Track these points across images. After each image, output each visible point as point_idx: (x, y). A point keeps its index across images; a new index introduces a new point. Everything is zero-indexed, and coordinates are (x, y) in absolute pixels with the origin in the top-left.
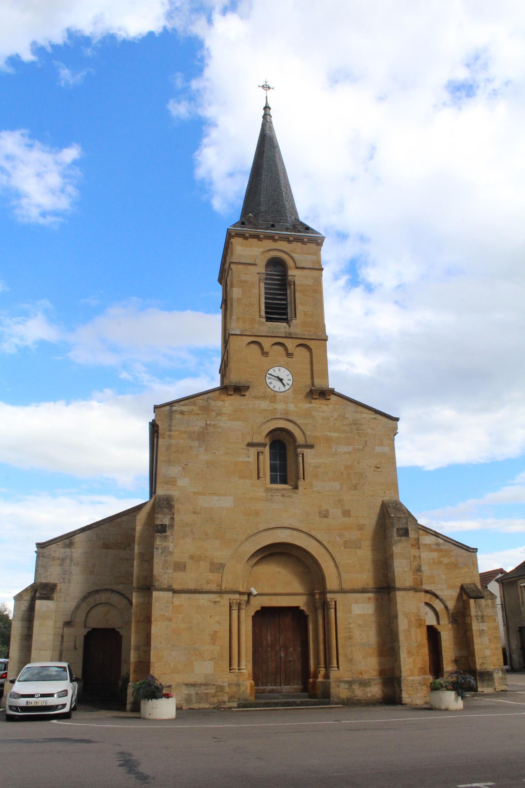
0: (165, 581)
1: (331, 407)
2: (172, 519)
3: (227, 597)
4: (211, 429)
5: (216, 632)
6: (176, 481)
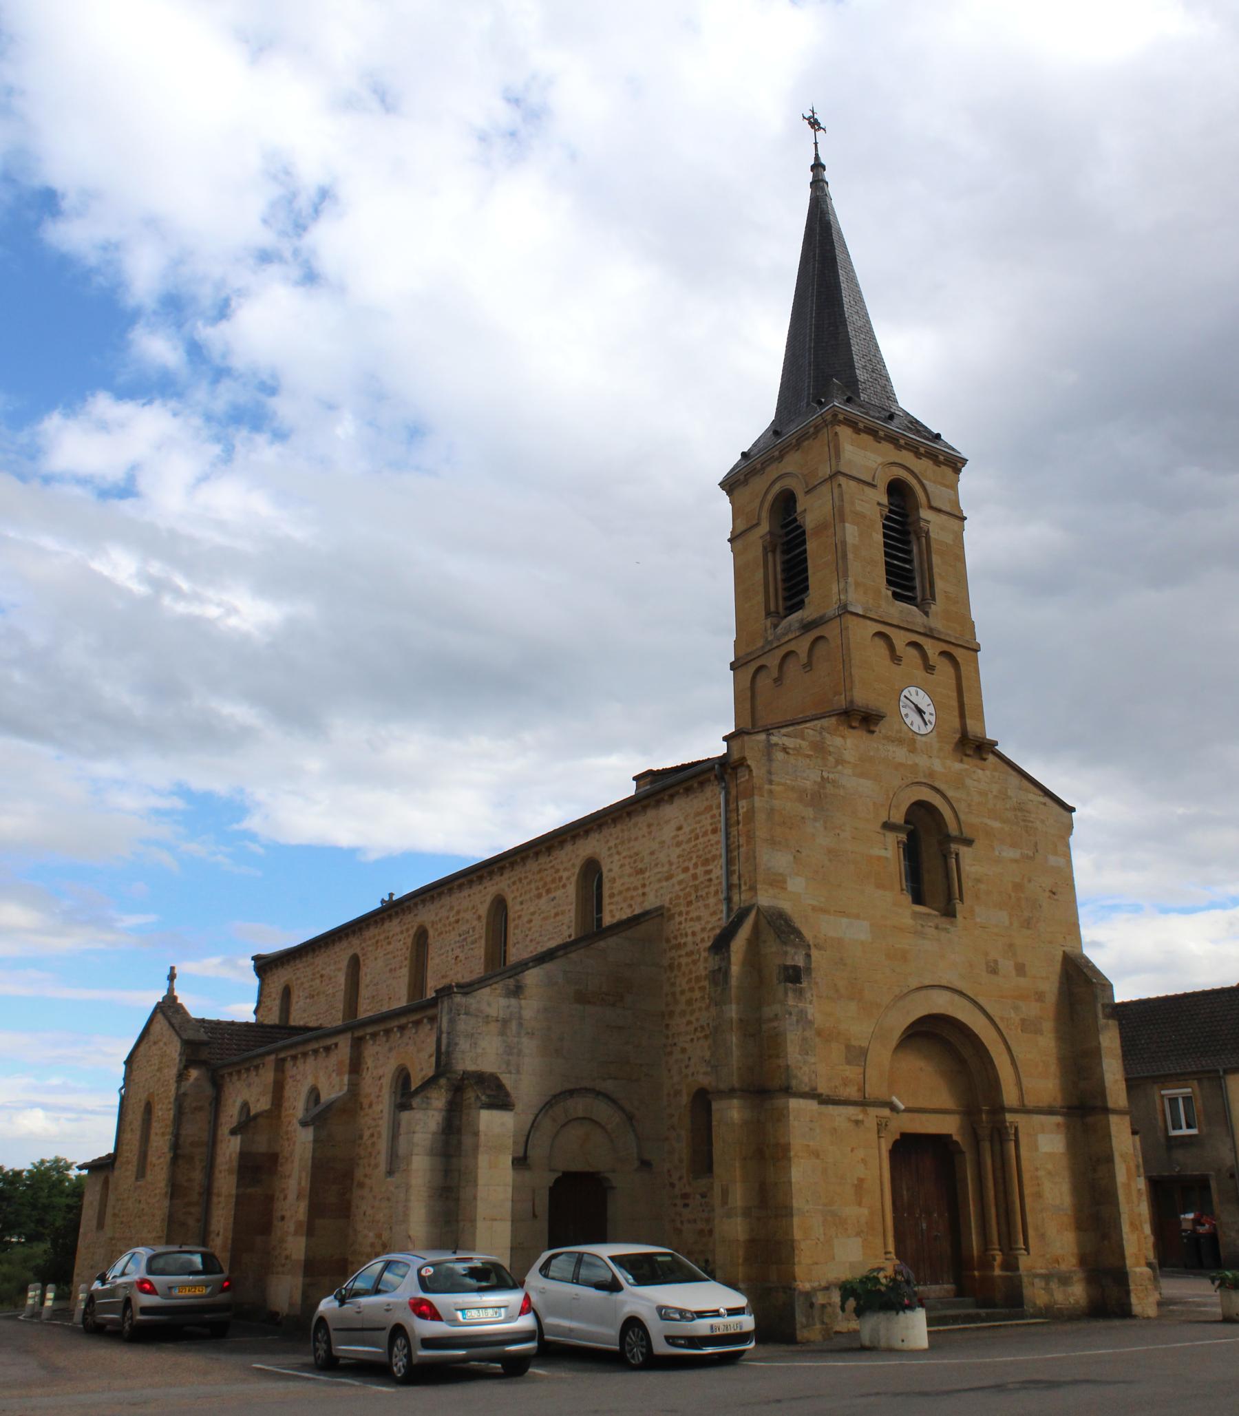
0: (806, 1079)
1: (988, 773)
2: (808, 956)
3: (873, 1112)
4: (830, 789)
5: (861, 1180)
6: (785, 882)
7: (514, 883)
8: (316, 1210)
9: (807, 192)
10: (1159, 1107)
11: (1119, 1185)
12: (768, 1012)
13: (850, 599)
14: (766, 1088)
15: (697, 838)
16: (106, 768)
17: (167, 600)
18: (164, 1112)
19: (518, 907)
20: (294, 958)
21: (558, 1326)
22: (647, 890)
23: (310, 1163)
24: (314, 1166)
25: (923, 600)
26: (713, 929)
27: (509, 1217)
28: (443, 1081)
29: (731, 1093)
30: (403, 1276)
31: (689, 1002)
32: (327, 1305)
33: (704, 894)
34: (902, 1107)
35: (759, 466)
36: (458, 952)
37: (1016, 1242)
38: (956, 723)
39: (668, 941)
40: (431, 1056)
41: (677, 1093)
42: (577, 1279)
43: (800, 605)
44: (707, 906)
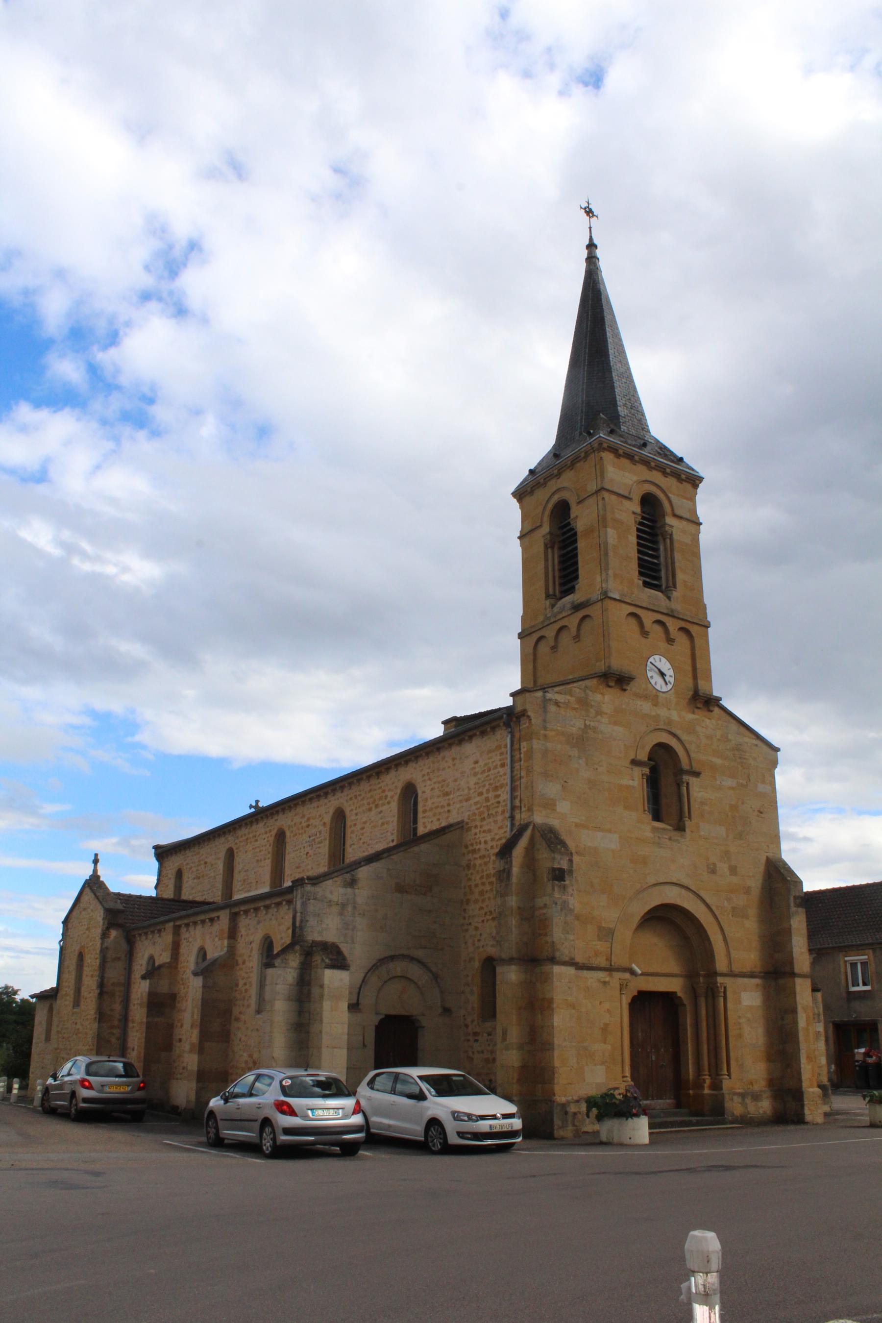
1: (713, 721)
2: (571, 861)
3: (618, 975)
5: (606, 1025)
6: (555, 805)
7: (351, 799)
8: (205, 1035)
9: (582, 267)
10: (842, 970)
11: (800, 1029)
12: (539, 902)
13: (609, 587)
14: (536, 958)
15: (489, 770)
16: (32, 692)
17: (76, 561)
18: (92, 961)
19: (353, 818)
20: (185, 849)
21: (381, 1123)
22: (451, 808)
23: (200, 1003)
24: (202, 1005)
25: (667, 587)
26: (500, 839)
27: (346, 1047)
28: (297, 947)
29: (511, 961)
30: (269, 1085)
31: (482, 893)
32: (215, 1102)
33: (494, 812)
34: (640, 972)
35: (542, 481)
36: (308, 849)
37: (721, 1069)
38: (690, 683)
39: (466, 847)
40: (288, 928)
41: (471, 959)
42: (395, 1091)
43: (571, 590)
44: (495, 822)
